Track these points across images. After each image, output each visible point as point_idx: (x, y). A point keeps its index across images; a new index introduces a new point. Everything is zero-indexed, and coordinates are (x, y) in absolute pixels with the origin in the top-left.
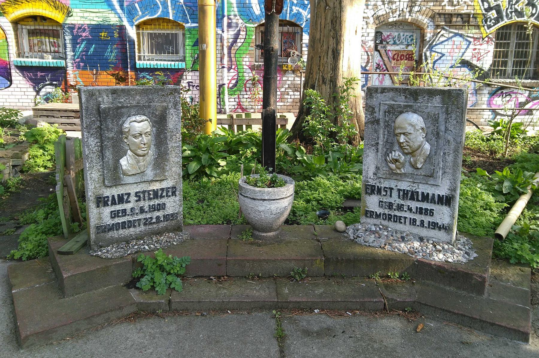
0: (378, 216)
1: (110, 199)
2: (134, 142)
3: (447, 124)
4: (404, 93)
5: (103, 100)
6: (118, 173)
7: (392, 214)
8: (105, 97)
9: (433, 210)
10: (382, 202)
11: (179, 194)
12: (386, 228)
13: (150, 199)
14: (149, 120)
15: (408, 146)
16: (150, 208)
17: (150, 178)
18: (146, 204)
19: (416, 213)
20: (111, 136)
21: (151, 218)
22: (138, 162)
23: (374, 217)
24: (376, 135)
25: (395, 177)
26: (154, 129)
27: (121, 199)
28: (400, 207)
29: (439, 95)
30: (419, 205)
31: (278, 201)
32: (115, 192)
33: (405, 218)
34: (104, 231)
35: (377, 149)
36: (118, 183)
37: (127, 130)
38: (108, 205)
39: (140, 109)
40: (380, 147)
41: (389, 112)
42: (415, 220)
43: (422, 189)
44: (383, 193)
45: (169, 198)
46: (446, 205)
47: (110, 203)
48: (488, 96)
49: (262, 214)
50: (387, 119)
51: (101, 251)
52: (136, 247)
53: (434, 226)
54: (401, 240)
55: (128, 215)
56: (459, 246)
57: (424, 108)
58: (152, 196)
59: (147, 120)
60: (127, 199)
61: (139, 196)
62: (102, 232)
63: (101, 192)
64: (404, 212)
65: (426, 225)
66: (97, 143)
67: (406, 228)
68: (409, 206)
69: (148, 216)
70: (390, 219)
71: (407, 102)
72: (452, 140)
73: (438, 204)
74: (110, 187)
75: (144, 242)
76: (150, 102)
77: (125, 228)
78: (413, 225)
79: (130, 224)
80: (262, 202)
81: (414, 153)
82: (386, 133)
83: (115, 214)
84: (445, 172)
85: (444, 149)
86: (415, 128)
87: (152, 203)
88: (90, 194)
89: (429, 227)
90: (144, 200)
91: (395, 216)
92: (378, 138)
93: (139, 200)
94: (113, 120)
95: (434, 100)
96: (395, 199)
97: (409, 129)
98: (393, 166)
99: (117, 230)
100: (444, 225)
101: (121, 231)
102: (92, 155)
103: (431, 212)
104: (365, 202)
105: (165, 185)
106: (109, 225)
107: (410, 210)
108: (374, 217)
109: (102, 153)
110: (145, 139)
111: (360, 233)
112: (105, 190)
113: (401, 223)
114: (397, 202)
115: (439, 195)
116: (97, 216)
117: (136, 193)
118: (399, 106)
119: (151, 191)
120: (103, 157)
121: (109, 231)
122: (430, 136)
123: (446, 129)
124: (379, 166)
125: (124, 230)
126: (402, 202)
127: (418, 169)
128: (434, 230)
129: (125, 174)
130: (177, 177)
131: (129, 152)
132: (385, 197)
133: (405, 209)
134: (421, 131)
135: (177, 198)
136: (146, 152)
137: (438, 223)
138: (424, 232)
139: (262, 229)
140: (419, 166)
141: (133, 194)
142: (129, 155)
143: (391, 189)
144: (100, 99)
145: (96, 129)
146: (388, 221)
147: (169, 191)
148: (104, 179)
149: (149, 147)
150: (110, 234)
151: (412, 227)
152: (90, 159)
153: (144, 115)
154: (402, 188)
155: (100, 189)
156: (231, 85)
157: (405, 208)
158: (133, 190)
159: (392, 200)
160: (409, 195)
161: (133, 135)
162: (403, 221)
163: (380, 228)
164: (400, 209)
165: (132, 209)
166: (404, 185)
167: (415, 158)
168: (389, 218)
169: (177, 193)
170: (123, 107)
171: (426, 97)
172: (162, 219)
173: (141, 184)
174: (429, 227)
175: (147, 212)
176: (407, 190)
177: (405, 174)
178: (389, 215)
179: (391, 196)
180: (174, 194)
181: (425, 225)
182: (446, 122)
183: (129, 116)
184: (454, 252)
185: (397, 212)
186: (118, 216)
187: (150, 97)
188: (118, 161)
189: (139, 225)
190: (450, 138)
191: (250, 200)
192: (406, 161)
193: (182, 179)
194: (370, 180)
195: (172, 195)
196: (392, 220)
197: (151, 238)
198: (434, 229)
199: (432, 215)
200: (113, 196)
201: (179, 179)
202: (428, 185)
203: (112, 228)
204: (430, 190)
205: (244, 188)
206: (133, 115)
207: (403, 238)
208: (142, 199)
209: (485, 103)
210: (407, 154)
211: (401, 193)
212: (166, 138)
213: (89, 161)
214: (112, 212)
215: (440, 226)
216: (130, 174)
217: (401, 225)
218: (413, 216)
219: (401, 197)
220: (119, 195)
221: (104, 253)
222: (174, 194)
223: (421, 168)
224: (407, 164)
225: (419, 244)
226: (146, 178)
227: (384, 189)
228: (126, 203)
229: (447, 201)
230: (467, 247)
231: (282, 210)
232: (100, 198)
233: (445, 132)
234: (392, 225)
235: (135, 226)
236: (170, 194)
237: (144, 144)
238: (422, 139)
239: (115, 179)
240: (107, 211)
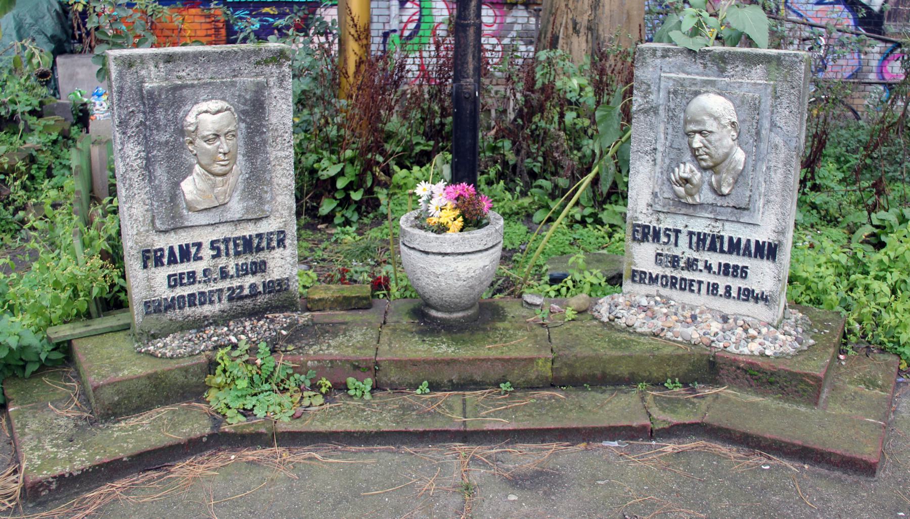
0: (653, 280)
1: (166, 253)
2: (206, 149)
3: (775, 116)
4: (703, 58)
5: (149, 74)
6: (178, 205)
7: (678, 276)
8: (152, 68)
9: (747, 267)
10: (660, 255)
11: (291, 244)
12: (666, 302)
13: (237, 254)
14: (233, 110)
15: (707, 154)
16: (237, 270)
17: (237, 216)
19: (719, 273)
20: (164, 139)
21: (241, 288)
22: (214, 186)
23: (647, 281)
24: (652, 134)
25: (683, 211)
26: (243, 125)
27: (185, 254)
28: (691, 265)
29: (762, 62)
30: (725, 259)
31: (470, 256)
32: (176, 241)
33: (700, 282)
35: (654, 160)
36: (179, 225)
37: (192, 128)
38: (163, 264)
39: (214, 89)
40: (659, 156)
41: (675, 92)
42: (715, 287)
43: (729, 231)
44: (664, 239)
45: (273, 252)
47: (165, 260)
48: (878, 57)
49: (441, 279)
50: (672, 106)
51: (153, 345)
52: (216, 338)
53: (747, 295)
54: (689, 320)
55: (200, 282)
56: (786, 328)
57: (736, 86)
58: (240, 249)
59: (229, 109)
60: (196, 254)
61: (218, 249)
62: (155, 312)
63: (149, 240)
64: (697, 273)
65: (734, 293)
66: (139, 152)
67: (701, 300)
68: (706, 262)
69: (236, 283)
70: (673, 285)
71: (707, 75)
72: (781, 144)
73: (756, 257)
74: (165, 232)
75: (229, 330)
76: (235, 76)
77: (195, 305)
78: (713, 294)
80: (440, 257)
81: (718, 168)
82: (670, 131)
84: (768, 201)
85: (769, 161)
86: (719, 123)
87: (241, 261)
88: (130, 247)
89: (739, 298)
90: (227, 254)
91: (682, 279)
92: (656, 140)
94: (167, 110)
95: (753, 71)
96: (683, 250)
97: (710, 125)
98: (681, 190)
99: (180, 308)
100: (763, 293)
101: (188, 311)
102: (131, 174)
103: (742, 271)
104: (631, 256)
105: (265, 227)
106: (166, 299)
107: (708, 268)
108: (647, 281)
109: (150, 172)
110: (224, 145)
111: (619, 312)
112: (156, 238)
113: (693, 291)
114: (687, 255)
115: (757, 242)
116: (144, 283)
117: (212, 243)
118: (694, 83)
119: (239, 238)
120: (150, 177)
121: (166, 309)
122: (746, 137)
123: (773, 125)
124: (657, 190)
125: (193, 309)
126: (695, 255)
127: (723, 195)
128: (746, 303)
129: (190, 208)
130: (286, 213)
131: (197, 168)
132: (666, 247)
133: (700, 268)
134: (729, 128)
135: (288, 252)
136: (228, 168)
137: (753, 291)
138: (731, 307)
139: (441, 306)
140: (725, 190)
141: (206, 245)
142: (198, 174)
143: (677, 232)
144: (143, 72)
145: (137, 127)
146: (671, 288)
147: (271, 240)
148: (153, 216)
149: (234, 160)
150: (170, 314)
151: (711, 297)
152: (128, 182)
153: (223, 99)
154: (696, 230)
155: (148, 236)
156: (406, 33)
157: (701, 266)
158: (206, 237)
159: (677, 252)
160: (708, 242)
161: (203, 137)
162: (695, 287)
163: (656, 302)
164: (692, 266)
165: (205, 271)
166: (700, 225)
167: (718, 177)
168: (673, 283)
169: (287, 242)
170: (182, 87)
171: (741, 67)
172: (261, 289)
173: (221, 226)
174: (739, 298)
175: (232, 277)
176: (705, 234)
177: (701, 204)
178: (673, 277)
179: (676, 245)
180: (281, 243)
181: (733, 295)
182: (772, 113)
183: (196, 103)
184: (776, 339)
185: (686, 272)
186: (182, 285)
187: (235, 66)
188: (177, 185)
189: (220, 300)
190: (778, 140)
191: (418, 254)
192: (703, 182)
193: (294, 217)
194: (641, 217)
195: (279, 246)
196: (678, 286)
197: (242, 323)
198: (747, 300)
199: (745, 277)
200: (171, 248)
201: (290, 216)
202: (739, 225)
203: (170, 305)
204: (743, 234)
205: (409, 232)
206: (204, 100)
207: (694, 317)
208: (223, 253)
209: (874, 69)
210: (705, 169)
211: (695, 239)
212: (265, 142)
213: (127, 186)
214: (169, 277)
216: (200, 207)
217: (692, 296)
218: (712, 279)
219: (694, 245)
220: (181, 247)
221: (160, 348)
222: (281, 243)
223: (728, 194)
224: (706, 187)
225: (720, 326)
226: (229, 216)
227: (665, 232)
228: (195, 260)
229: (768, 251)
230: (800, 330)
231: (477, 272)
232: (148, 251)
233: (771, 130)
234: (677, 296)
235: (212, 302)
236: (274, 244)
237: (225, 154)
238: (731, 142)
239: (173, 218)
240: (161, 274)
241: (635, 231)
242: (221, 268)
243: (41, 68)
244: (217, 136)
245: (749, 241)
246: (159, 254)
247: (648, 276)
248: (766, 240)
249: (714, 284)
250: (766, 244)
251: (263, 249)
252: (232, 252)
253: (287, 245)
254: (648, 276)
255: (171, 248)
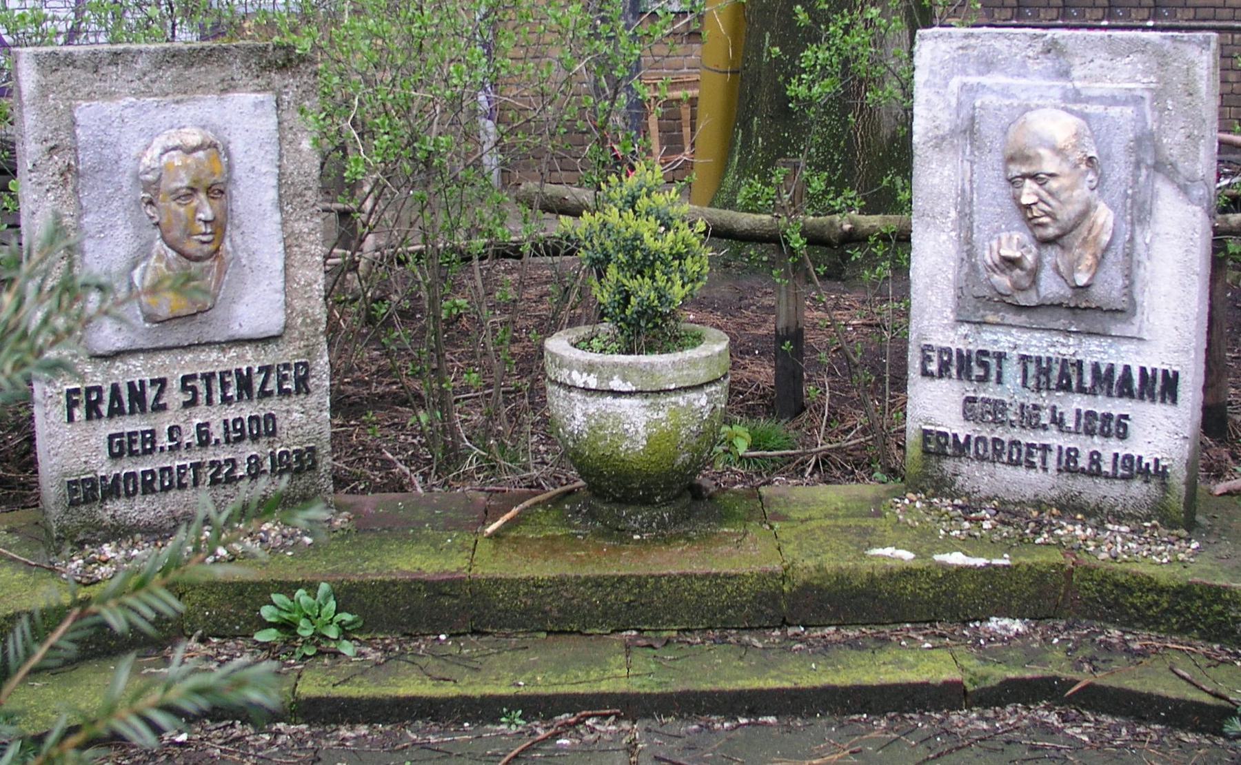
1: (107, 396)
7: (1006, 438)
9: (1126, 417)
10: (974, 400)
13: (226, 400)
15: (1047, 214)
18: (217, 417)
21: (232, 462)
30: (1080, 403)
33: (1046, 448)
34: (89, 499)
38: (100, 416)
43: (1093, 352)
44: (978, 371)
46: (1163, 401)
47: (104, 409)
60: (157, 398)
61: (194, 389)
62: (86, 502)
68: (1054, 409)
73: (1141, 398)
79: (173, 481)
81: (1066, 240)
83: (120, 444)
87: (231, 413)
90: (209, 401)
91: (1015, 443)
93: (193, 403)
96: (1010, 389)
103: (1119, 424)
106: (104, 478)
107: (1058, 421)
117: (185, 379)
126: (1032, 399)
134: (1083, 167)
137: (1140, 458)
143: (1001, 357)
154: (1033, 352)
157: (1045, 418)
176: (1049, 359)
178: (995, 440)
186: (133, 453)
195: (298, 392)
200: (115, 389)
203: (113, 489)
211: (1032, 369)
214: (111, 437)
215: (1148, 465)
218: (1067, 442)
222: (302, 385)
236: (290, 385)
237: (206, 222)
241: (926, 359)
242: (199, 426)
243: (1191, 317)
244: (193, 191)
245: (1127, 368)
246: (94, 397)
247: (951, 441)
248: (1160, 367)
249: (1069, 449)
250: (1160, 374)
251: (270, 394)
252: (217, 397)
253: (312, 388)
254: (951, 441)
255: (115, 389)
